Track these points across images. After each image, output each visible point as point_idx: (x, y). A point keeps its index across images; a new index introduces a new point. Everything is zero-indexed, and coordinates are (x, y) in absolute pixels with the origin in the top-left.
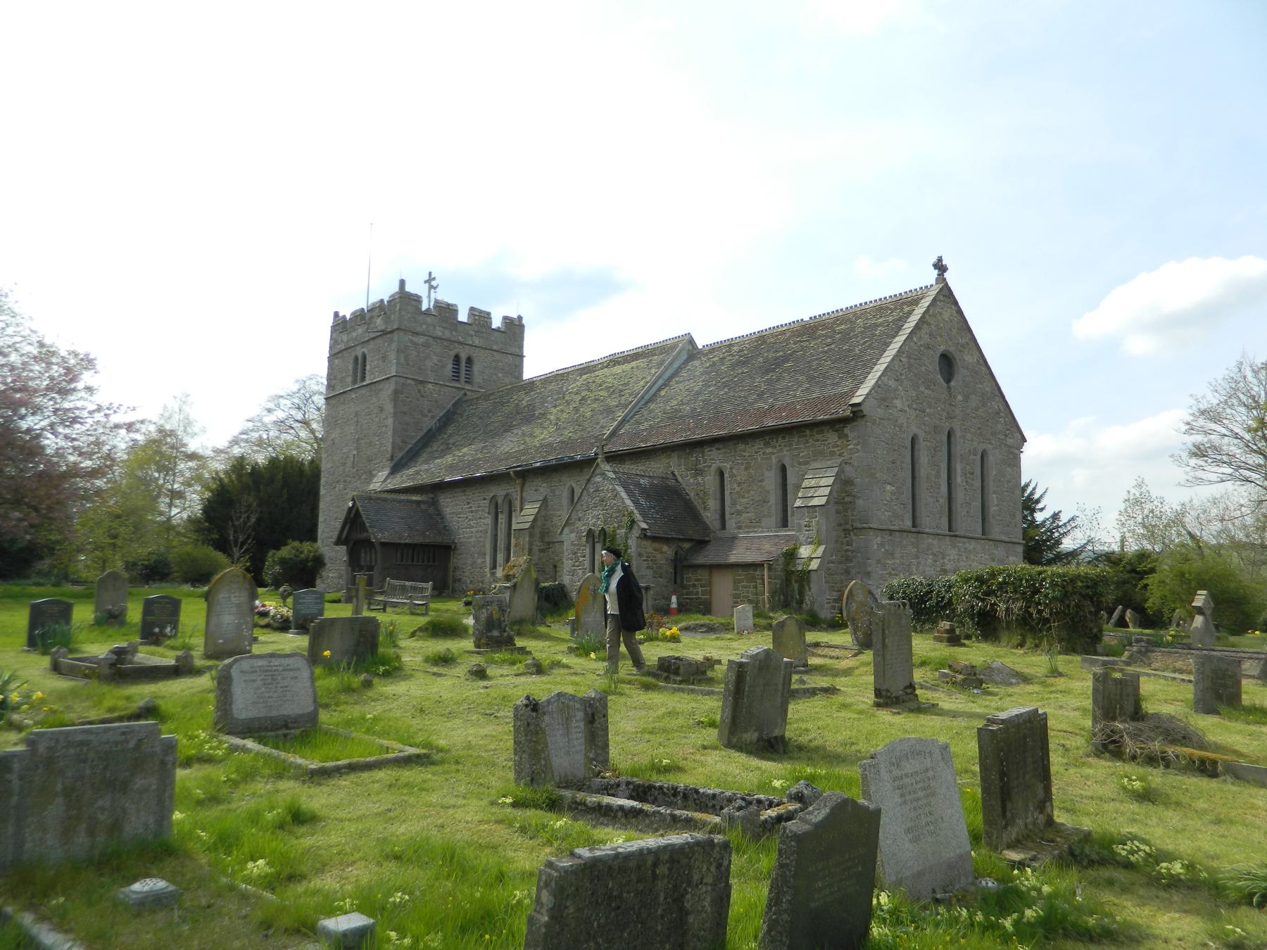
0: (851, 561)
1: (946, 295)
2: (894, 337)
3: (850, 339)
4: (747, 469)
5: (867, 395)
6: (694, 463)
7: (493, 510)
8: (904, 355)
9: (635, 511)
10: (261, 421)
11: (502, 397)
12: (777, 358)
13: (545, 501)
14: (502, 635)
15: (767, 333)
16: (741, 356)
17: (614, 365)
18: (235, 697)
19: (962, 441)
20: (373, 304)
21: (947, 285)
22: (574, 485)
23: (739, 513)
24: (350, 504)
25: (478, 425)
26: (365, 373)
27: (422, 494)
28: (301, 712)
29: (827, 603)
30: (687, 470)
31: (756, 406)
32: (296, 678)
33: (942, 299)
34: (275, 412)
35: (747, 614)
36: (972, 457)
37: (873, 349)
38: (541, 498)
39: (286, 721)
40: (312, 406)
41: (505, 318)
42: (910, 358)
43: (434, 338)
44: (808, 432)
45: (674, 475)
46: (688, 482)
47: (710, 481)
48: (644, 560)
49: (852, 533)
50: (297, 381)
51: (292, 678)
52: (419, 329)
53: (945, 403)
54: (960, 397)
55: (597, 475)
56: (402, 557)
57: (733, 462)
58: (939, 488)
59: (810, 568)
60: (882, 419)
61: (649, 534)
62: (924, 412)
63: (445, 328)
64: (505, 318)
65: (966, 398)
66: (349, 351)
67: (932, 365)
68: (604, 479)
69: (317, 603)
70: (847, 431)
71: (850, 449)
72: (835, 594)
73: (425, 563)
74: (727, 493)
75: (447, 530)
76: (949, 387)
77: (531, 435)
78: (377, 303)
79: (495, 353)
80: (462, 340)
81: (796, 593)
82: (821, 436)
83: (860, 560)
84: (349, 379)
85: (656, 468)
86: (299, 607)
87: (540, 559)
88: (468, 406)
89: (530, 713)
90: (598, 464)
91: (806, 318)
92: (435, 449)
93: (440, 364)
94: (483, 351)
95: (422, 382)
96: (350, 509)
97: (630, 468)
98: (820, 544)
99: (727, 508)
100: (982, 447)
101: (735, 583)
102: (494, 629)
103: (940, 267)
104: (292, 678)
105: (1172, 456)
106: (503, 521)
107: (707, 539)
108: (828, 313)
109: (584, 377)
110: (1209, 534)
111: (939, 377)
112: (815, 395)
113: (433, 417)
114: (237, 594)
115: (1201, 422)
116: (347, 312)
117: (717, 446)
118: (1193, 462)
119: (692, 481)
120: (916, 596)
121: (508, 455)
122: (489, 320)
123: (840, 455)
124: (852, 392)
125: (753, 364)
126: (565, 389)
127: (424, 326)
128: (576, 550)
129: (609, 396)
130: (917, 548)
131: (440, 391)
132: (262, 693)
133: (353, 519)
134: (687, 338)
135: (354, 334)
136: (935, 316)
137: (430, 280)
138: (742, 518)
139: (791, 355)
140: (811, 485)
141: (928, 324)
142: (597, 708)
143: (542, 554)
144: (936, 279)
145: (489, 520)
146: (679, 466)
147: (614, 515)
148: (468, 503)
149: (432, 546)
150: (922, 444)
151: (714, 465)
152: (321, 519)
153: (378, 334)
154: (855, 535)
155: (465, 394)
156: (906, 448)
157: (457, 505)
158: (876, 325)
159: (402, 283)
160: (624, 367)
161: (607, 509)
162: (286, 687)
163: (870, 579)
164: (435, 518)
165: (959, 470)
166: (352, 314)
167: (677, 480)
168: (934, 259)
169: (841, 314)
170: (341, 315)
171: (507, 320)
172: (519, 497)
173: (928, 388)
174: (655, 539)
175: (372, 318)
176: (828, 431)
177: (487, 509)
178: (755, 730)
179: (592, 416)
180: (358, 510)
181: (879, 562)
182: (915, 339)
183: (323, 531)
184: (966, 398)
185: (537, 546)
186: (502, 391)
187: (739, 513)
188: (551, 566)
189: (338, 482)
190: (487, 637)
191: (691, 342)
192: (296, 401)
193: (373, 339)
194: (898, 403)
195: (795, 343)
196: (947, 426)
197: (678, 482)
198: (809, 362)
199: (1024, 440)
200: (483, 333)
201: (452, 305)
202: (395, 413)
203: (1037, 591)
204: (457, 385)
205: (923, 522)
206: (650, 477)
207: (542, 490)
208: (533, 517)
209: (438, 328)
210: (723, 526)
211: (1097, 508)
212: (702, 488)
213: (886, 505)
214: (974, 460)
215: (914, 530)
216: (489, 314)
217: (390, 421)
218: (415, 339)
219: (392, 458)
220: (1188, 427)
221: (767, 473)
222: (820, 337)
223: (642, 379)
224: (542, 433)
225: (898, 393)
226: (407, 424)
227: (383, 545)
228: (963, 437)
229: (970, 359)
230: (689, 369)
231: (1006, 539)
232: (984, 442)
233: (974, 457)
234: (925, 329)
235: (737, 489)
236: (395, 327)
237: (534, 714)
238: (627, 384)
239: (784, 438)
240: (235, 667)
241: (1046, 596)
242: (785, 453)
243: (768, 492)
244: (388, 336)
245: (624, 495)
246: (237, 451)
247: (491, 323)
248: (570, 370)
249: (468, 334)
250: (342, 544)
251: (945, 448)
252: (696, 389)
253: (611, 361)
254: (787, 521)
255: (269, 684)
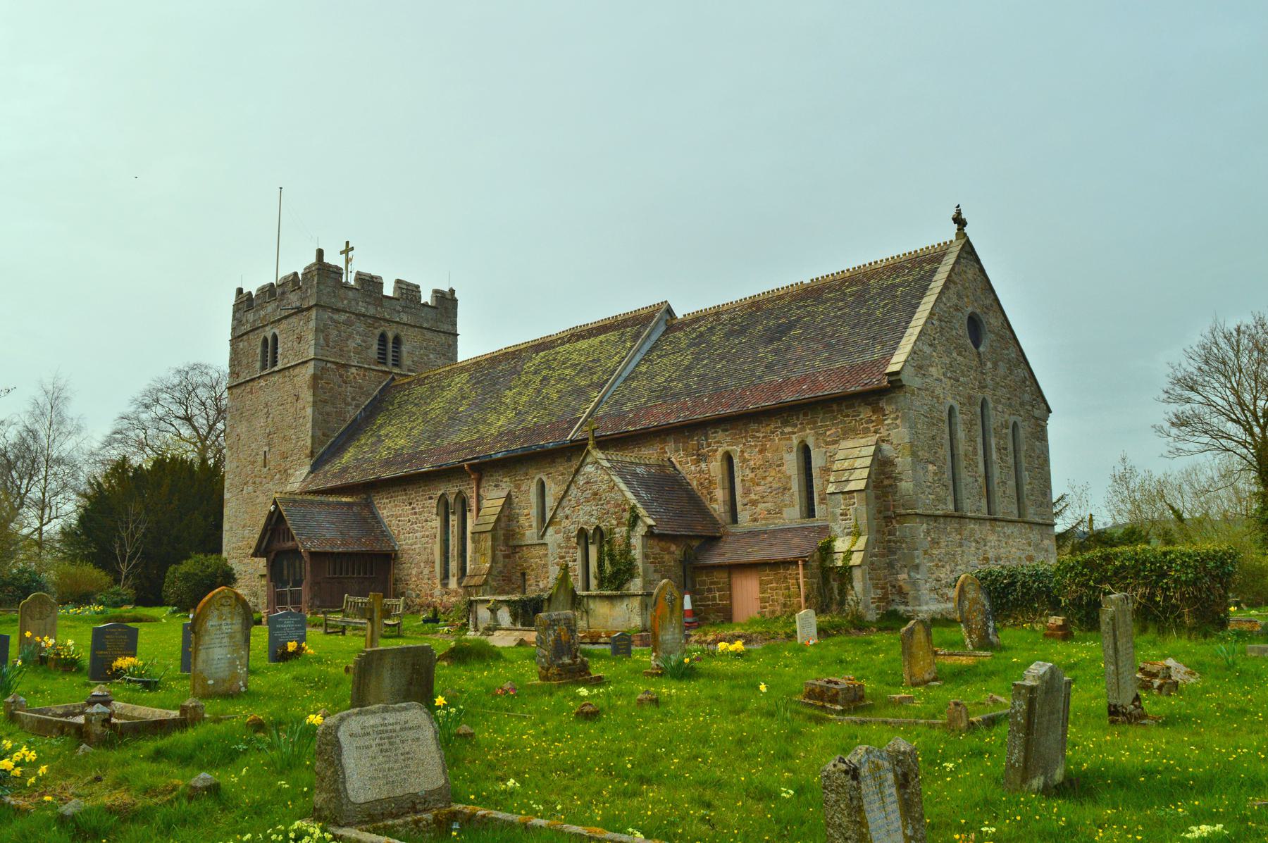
0: (895, 553)
1: (968, 252)
2: (922, 298)
3: (866, 301)
4: (761, 451)
5: (905, 361)
6: (696, 448)
7: (442, 512)
8: (936, 317)
9: (638, 505)
10: (138, 419)
11: (440, 380)
12: (780, 326)
13: (509, 497)
14: (575, 663)
15: (761, 298)
16: (734, 325)
17: (577, 340)
18: (348, 772)
19: (994, 412)
20: (285, 278)
21: (968, 240)
22: (544, 479)
23: (754, 503)
24: (272, 508)
25: (414, 414)
26: (277, 357)
27: (352, 496)
28: (430, 787)
29: (872, 603)
30: (687, 456)
31: (767, 379)
32: (418, 739)
33: (965, 256)
34: (153, 408)
35: (811, 620)
36: (1004, 431)
37: (897, 311)
38: (504, 494)
39: (414, 803)
40: (196, 399)
41: (436, 292)
42: (941, 321)
43: (357, 315)
44: (835, 407)
45: (672, 462)
46: (687, 467)
47: (715, 467)
48: (651, 563)
49: (894, 521)
50: (179, 372)
51: (413, 740)
52: (340, 305)
53: (976, 370)
54: (989, 365)
55: (588, 464)
56: (335, 569)
57: (744, 444)
58: (976, 467)
59: (851, 563)
60: (919, 389)
61: (656, 532)
62: (958, 381)
63: (369, 303)
64: (436, 292)
65: (995, 365)
66: (256, 332)
67: (961, 329)
68: (597, 468)
69: (297, 629)
70: (882, 404)
71: (888, 425)
72: (879, 591)
73: (361, 575)
74: (738, 481)
75: (386, 536)
76: (979, 354)
77: (485, 422)
78: (289, 276)
79: (425, 332)
80: (388, 317)
81: (836, 592)
82: (851, 411)
83: (906, 551)
84: (258, 365)
85: (650, 454)
86: (277, 634)
87: (505, 566)
88: (399, 392)
89: (851, 782)
90: (588, 452)
91: (807, 281)
92: (363, 442)
93: (363, 344)
94: (411, 329)
95: (344, 366)
96: (271, 514)
97: (628, 456)
98: (858, 534)
99: (738, 498)
100: (1013, 419)
101: (760, 584)
102: (564, 654)
103: (959, 221)
104: (413, 740)
105: (1154, 427)
106: (456, 523)
107: (718, 534)
108: (833, 275)
109: (542, 354)
110: (1189, 506)
111: (969, 341)
112: (838, 365)
113: (357, 406)
114: (229, 621)
115: (1178, 390)
116: (252, 287)
117: (723, 426)
118: (1174, 431)
119: (693, 468)
120: (996, 588)
121: (459, 447)
122: (418, 294)
123: (876, 432)
124: (886, 360)
125: (751, 333)
126: (518, 368)
127: (345, 302)
128: (563, 554)
129: (577, 374)
130: (960, 534)
131: (365, 375)
132: (379, 764)
133: (275, 525)
134: (664, 307)
135: (262, 313)
136: (960, 274)
137: (348, 250)
138: (758, 509)
139: (795, 321)
140: (844, 467)
141: (955, 283)
142: (909, 765)
143: (507, 560)
144: (957, 234)
145: (437, 523)
146: (676, 451)
147: (612, 510)
148: (410, 504)
149: (369, 554)
150: (959, 418)
151: (720, 449)
152: (226, 526)
153: (293, 311)
154: (898, 522)
155: (393, 379)
156: (944, 421)
157: (396, 506)
158: (894, 286)
159: (320, 253)
160: (590, 341)
161: (602, 505)
162: (408, 753)
163: (918, 573)
164: (371, 523)
165: (993, 446)
166: (258, 290)
167: (674, 467)
168: (953, 212)
169: (848, 274)
170: (245, 291)
171: (438, 294)
172: (474, 495)
173: (960, 354)
174: (661, 537)
175: (283, 293)
176: (859, 405)
177: (435, 510)
178: (1042, 774)
179: (560, 398)
180: (280, 512)
181: (926, 552)
182: (944, 299)
183: (227, 546)
184: (995, 365)
185: (501, 551)
186: (440, 374)
187: (754, 503)
188: (519, 575)
189: (245, 484)
190: (558, 666)
191: (669, 311)
192: (177, 394)
193: (286, 317)
194: (933, 370)
195: (798, 308)
196: (980, 395)
197: (678, 470)
198: (821, 329)
199: (1049, 411)
200: (411, 308)
201: (376, 278)
202: (315, 403)
203: (1164, 575)
204: (384, 368)
205: (965, 505)
206: (646, 465)
207: (504, 485)
208: (496, 516)
209: (360, 304)
210: (734, 520)
211: (1085, 484)
212: (707, 476)
213: (929, 487)
214: (1006, 434)
215: (956, 514)
216: (417, 287)
217: (309, 411)
218: (336, 317)
219: (312, 454)
220: (1167, 395)
221: (787, 457)
222: (828, 300)
223: (616, 354)
224: (499, 419)
225: (933, 359)
226: (328, 414)
227: (313, 555)
228: (995, 409)
229: (995, 322)
230: (671, 342)
231: (1041, 521)
232: (1014, 414)
233: (1007, 431)
234: (953, 289)
235: (751, 475)
236: (312, 303)
237: (855, 783)
238: (598, 360)
239: (805, 414)
240: (342, 729)
241: (1177, 581)
242: (808, 431)
243: (789, 477)
244: (305, 313)
245: (623, 486)
246: (115, 454)
247: (420, 298)
248: (522, 347)
249: (395, 309)
250: (262, 556)
251: (979, 422)
252: (686, 363)
253: (572, 335)
254: (813, 510)
255: (386, 751)
